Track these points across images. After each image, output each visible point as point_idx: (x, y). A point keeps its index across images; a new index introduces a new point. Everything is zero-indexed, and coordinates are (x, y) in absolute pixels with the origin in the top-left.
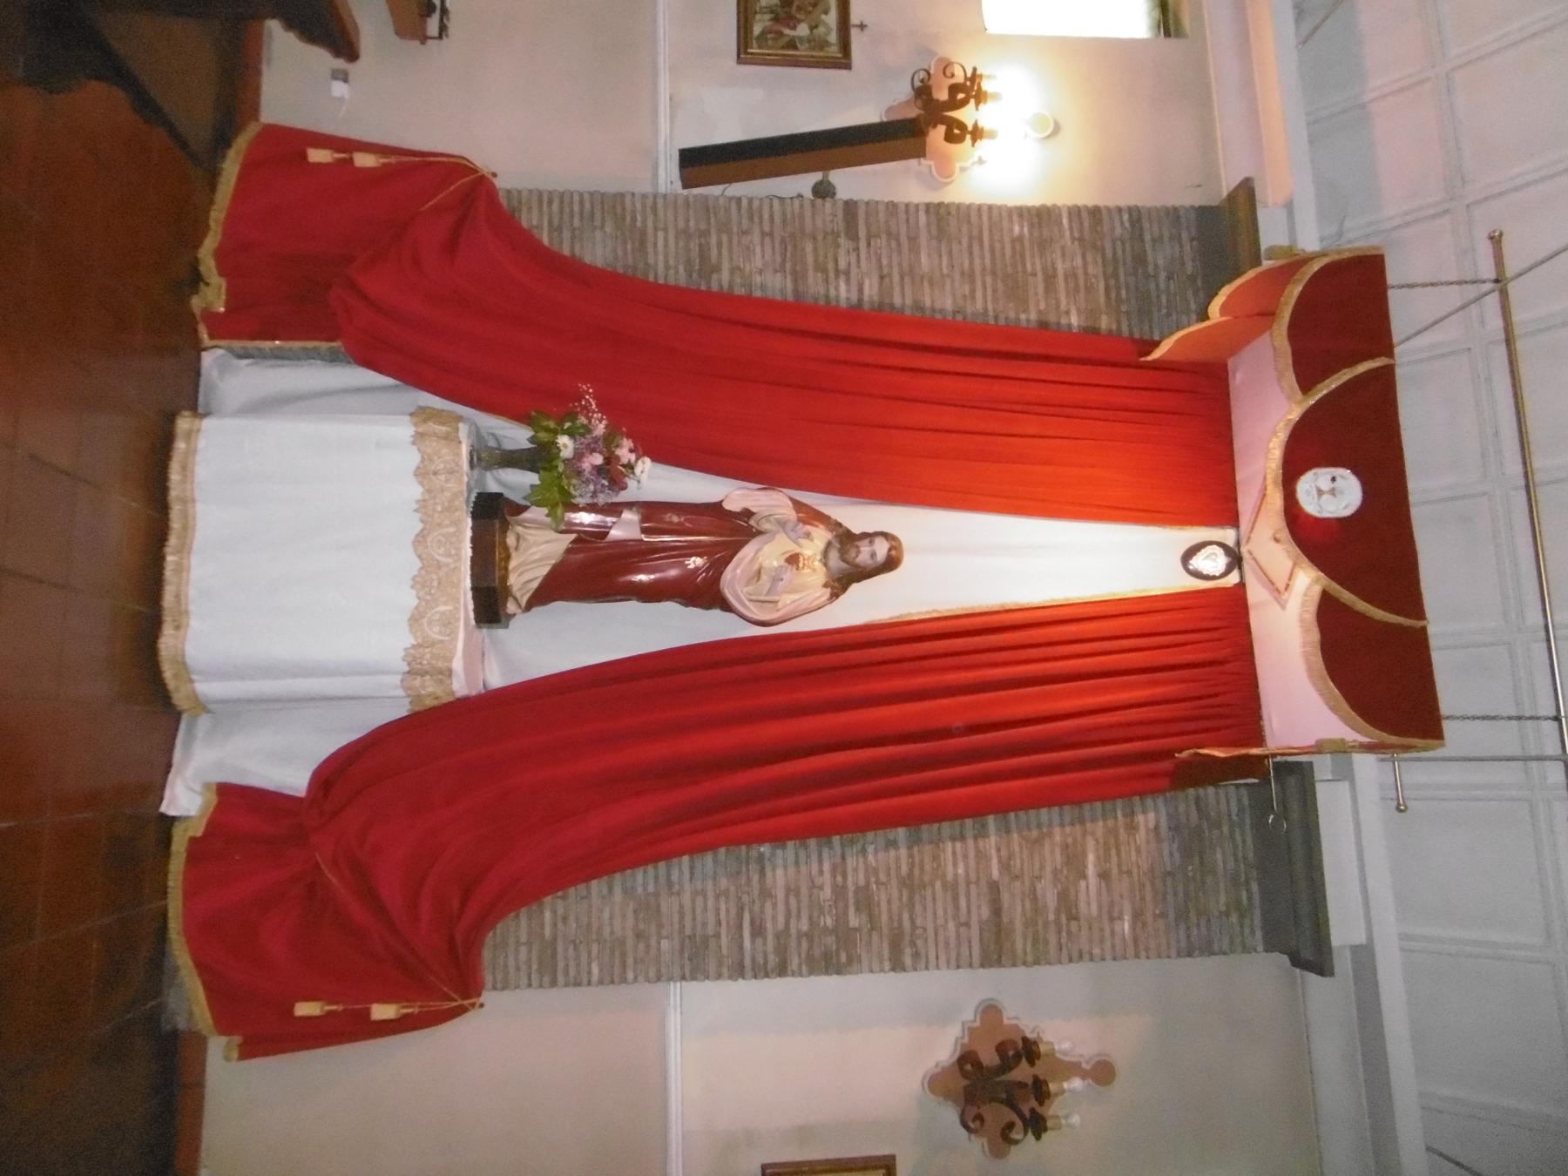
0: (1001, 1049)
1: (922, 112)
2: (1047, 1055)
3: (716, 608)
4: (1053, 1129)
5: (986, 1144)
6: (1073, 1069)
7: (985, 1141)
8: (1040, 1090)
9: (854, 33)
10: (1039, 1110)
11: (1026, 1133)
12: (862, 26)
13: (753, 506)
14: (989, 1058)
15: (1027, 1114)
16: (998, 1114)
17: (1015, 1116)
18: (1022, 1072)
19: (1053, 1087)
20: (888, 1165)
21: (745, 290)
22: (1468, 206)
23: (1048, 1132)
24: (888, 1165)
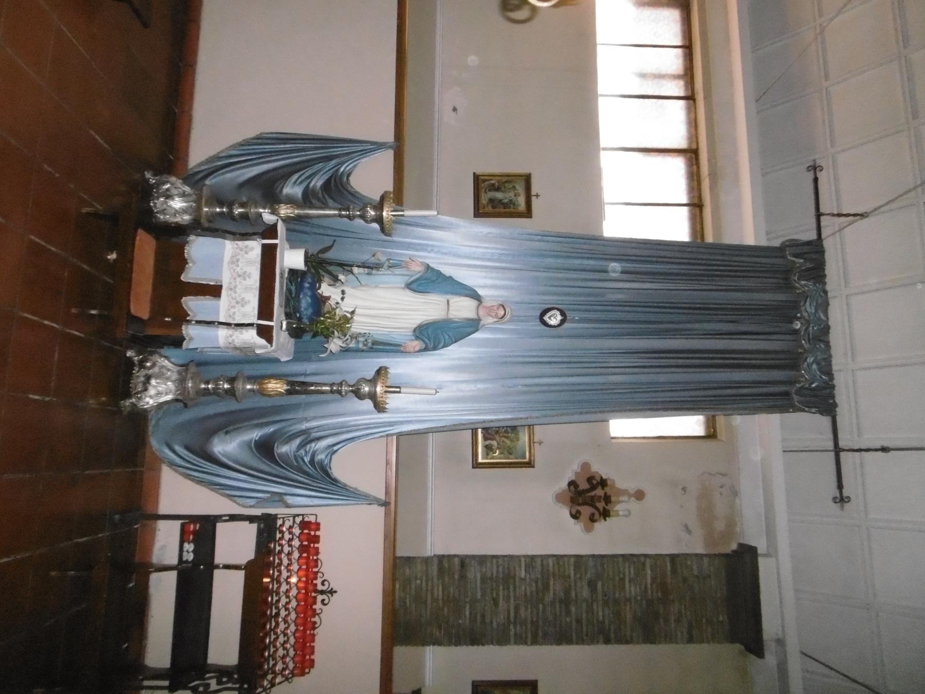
0: (590, 479)
1: (115, 252)
2: (610, 485)
3: (152, 668)
4: (613, 516)
5: (583, 526)
6: (624, 492)
7: (582, 524)
8: (607, 499)
9: (533, 198)
10: (606, 507)
11: (600, 516)
12: (540, 443)
13: (433, 263)
14: (583, 485)
15: (601, 509)
16: (586, 511)
17: (594, 509)
18: (599, 492)
19: (613, 499)
20: (532, 686)
21: (183, 195)
22: (847, 296)
23: (611, 518)
24: (532, 686)
